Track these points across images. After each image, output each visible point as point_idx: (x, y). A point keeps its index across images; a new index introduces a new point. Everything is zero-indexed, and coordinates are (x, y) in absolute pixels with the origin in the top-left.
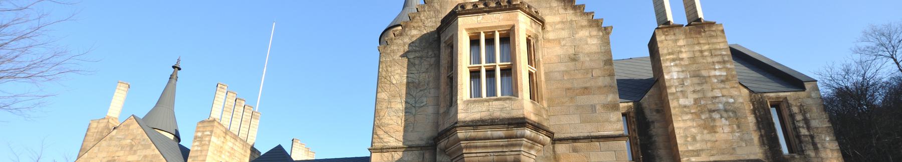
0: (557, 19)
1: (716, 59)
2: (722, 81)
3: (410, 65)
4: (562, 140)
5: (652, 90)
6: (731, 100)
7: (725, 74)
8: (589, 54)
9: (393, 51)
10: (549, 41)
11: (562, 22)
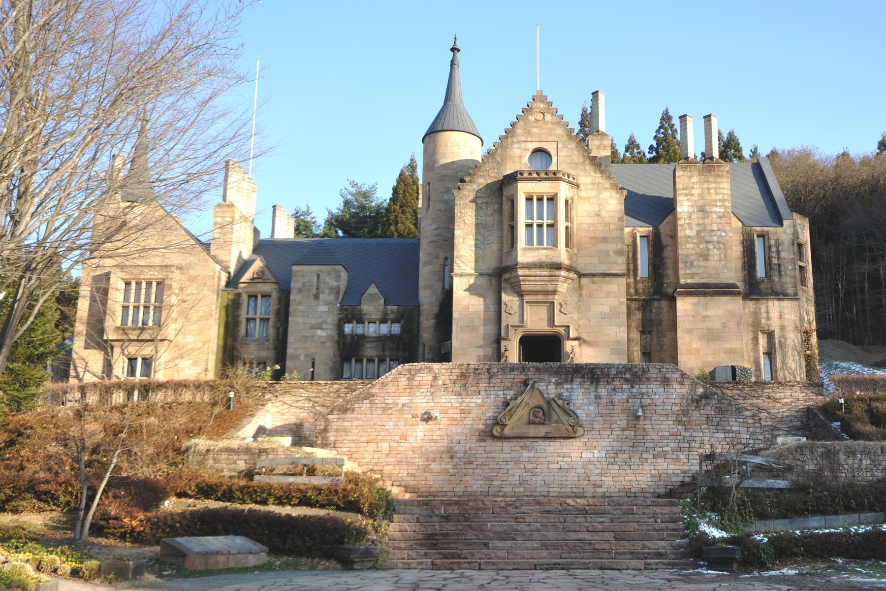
0: (589, 180)
1: (719, 197)
2: (720, 217)
3: (478, 209)
4: (585, 275)
5: (669, 217)
6: (724, 234)
7: (722, 210)
8: (608, 212)
9: (465, 196)
10: (582, 198)
11: (593, 184)
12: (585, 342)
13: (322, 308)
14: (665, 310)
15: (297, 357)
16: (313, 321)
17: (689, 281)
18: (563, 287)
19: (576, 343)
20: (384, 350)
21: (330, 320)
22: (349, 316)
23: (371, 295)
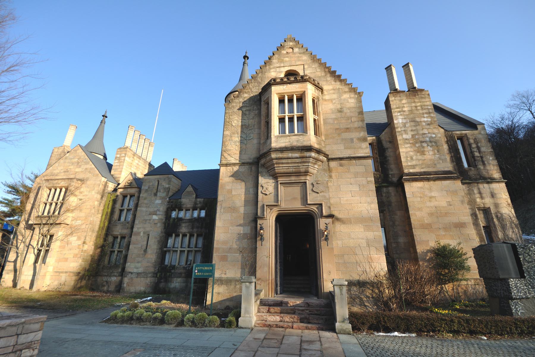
0: (331, 87)
1: (425, 111)
2: (428, 124)
3: (243, 114)
5: (387, 129)
6: (434, 136)
8: (349, 108)
9: (233, 107)
10: (326, 100)
11: (334, 89)
12: (338, 219)
13: (158, 201)
14: (393, 194)
15: (139, 233)
16: (152, 210)
17: (411, 171)
18: (314, 169)
19: (329, 220)
20: (193, 228)
21: (161, 209)
22: (174, 206)
23: (188, 192)
